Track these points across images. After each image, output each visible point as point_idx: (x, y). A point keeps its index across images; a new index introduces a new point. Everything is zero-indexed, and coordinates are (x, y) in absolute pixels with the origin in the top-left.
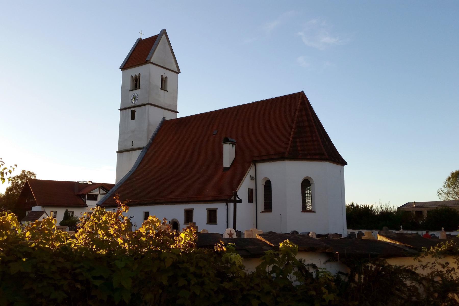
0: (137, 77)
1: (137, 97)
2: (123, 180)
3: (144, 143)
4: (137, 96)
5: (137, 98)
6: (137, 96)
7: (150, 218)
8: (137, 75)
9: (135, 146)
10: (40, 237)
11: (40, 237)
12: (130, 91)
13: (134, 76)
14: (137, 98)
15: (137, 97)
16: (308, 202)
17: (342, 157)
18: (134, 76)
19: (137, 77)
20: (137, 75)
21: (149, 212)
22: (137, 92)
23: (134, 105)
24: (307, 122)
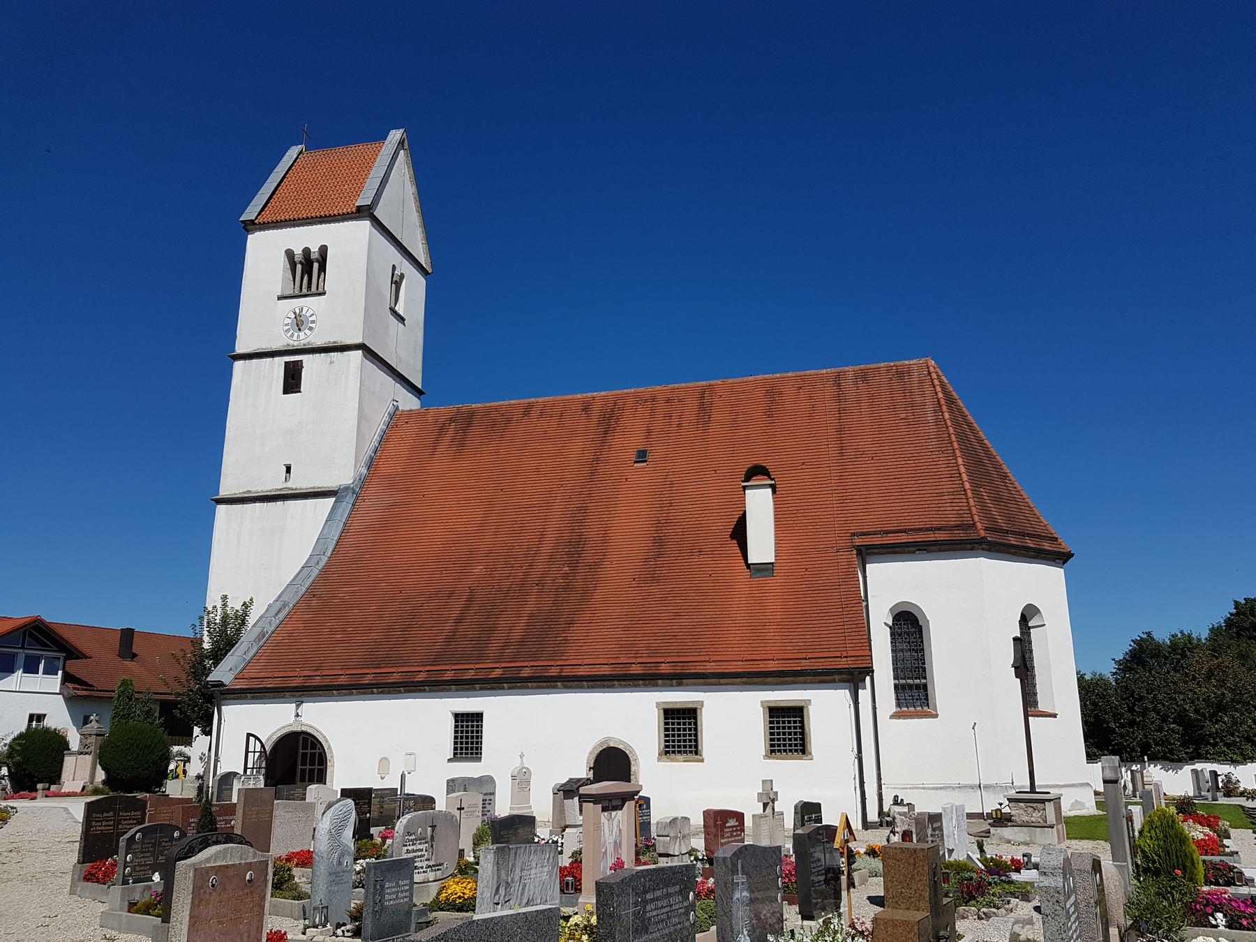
0: (315, 255)
1: (311, 319)
2: (410, 260)
3: (344, 472)
4: (313, 315)
5: (313, 322)
6: (313, 315)
7: (297, 872)
8: (315, 249)
9: (299, 482)
10: (1238, 740)
11: (1238, 740)
12: (280, 298)
13: (298, 251)
14: (313, 322)
15: (313, 318)
16: (388, 888)
17: (930, 560)
18: (298, 251)
19: (313, 256)
20: (315, 249)
21: (482, 714)
22: (309, 305)
23: (295, 343)
24: (735, 545)
